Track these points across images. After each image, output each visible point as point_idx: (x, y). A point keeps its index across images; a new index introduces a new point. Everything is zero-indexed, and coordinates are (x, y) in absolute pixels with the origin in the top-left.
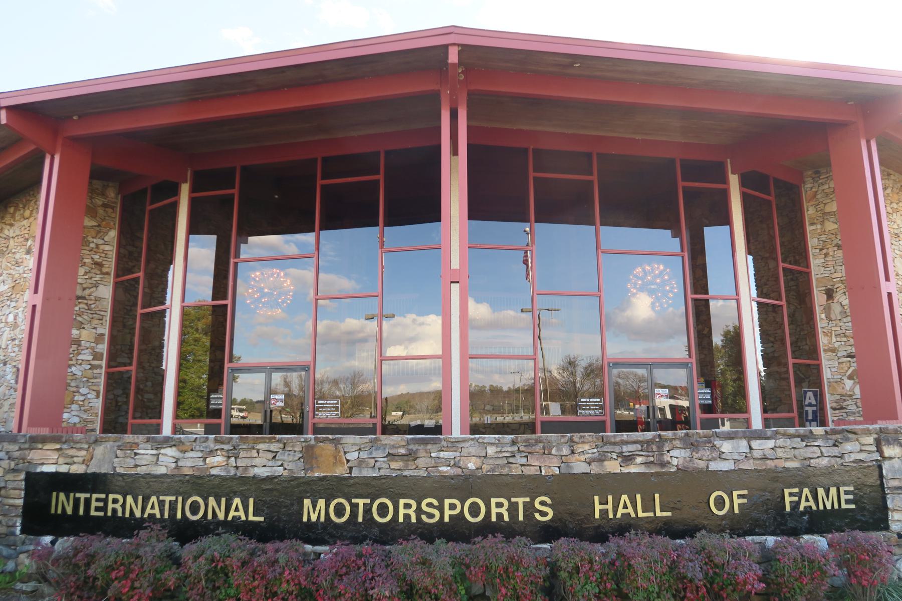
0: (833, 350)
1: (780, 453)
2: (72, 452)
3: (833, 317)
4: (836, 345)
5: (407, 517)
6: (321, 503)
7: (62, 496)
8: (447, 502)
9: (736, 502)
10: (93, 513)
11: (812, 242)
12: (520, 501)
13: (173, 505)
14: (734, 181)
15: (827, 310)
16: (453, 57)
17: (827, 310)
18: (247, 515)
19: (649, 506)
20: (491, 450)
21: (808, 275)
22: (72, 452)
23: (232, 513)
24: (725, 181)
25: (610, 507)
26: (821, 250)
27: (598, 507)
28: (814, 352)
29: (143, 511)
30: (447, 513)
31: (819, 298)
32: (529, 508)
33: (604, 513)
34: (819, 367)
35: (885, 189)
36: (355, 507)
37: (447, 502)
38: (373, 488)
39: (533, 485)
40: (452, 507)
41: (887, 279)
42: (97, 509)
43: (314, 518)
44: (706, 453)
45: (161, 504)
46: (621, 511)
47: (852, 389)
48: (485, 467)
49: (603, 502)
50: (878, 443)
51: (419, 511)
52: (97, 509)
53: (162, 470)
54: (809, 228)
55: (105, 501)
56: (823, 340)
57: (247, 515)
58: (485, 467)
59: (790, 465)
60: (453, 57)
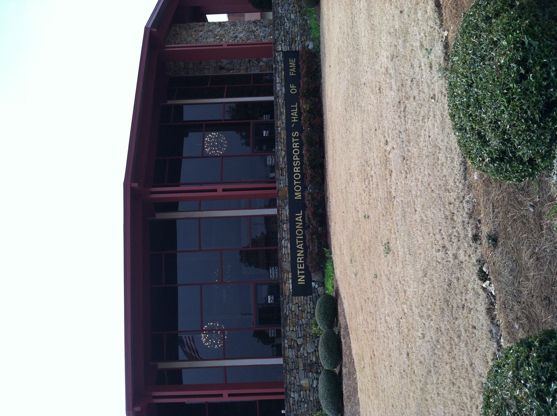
0: (247, 69)
1: (280, 76)
2: (285, 278)
3: (232, 68)
4: (244, 67)
5: (299, 170)
6: (296, 194)
7: (299, 280)
8: (294, 159)
9: (293, 87)
10: (303, 268)
11: (197, 74)
12: (293, 140)
13: (299, 240)
14: (170, 102)
15: (229, 70)
16: (135, 185)
17: (229, 70)
18: (300, 216)
19: (294, 108)
20: (280, 148)
21: (212, 76)
22: (285, 278)
23: (300, 220)
24: (171, 106)
25: (295, 118)
26: (201, 70)
27: (295, 121)
28: (247, 77)
29: (301, 250)
30: (297, 159)
31: (223, 73)
32: (295, 138)
33: (296, 119)
34: (254, 74)
35: (176, 44)
36: (297, 184)
37: (294, 159)
38: (291, 180)
39: (289, 137)
40: (295, 158)
41: (222, 45)
42: (302, 266)
43: (300, 196)
44: (280, 94)
45: (299, 244)
46: (296, 115)
47: (264, 62)
48: (285, 149)
49: (293, 119)
50: (278, 52)
51: (297, 166)
52: (302, 266)
53: (289, 244)
54: (191, 75)
55: (299, 263)
56: (242, 72)
57: (300, 216)
58: (285, 149)
59: (283, 74)
60: (135, 185)
